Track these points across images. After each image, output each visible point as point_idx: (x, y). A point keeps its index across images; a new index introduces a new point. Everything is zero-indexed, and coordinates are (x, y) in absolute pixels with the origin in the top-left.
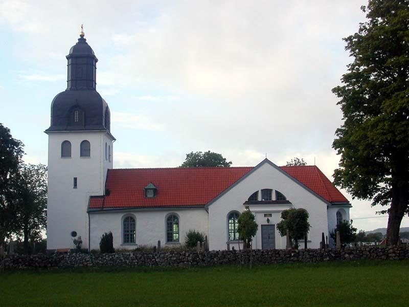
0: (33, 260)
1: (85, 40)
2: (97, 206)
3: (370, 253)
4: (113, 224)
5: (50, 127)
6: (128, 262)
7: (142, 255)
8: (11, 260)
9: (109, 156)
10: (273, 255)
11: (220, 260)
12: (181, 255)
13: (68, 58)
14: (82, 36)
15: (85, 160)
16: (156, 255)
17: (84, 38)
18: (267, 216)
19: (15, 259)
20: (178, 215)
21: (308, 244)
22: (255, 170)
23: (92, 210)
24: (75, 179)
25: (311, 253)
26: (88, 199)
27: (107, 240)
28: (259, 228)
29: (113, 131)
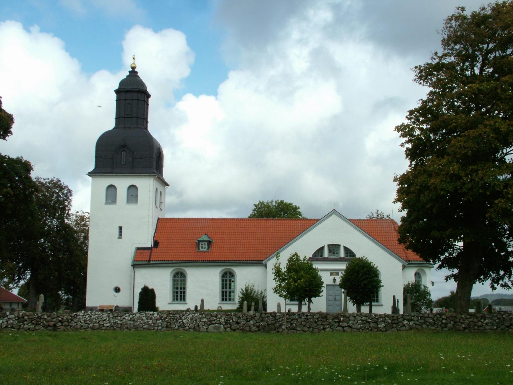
0: (41, 318)
1: (137, 72)
2: (144, 259)
3: (433, 320)
4: (160, 281)
5: (94, 170)
6: (151, 322)
7: (168, 315)
8: (15, 317)
9: (160, 203)
10: (320, 319)
11: (257, 323)
12: (212, 316)
13: (117, 92)
14: (133, 68)
15: (132, 207)
16: (183, 315)
17: (136, 70)
18: (334, 275)
19: (21, 317)
20: (234, 271)
21: (373, 308)
22: (321, 222)
23: (137, 263)
24: (121, 228)
25: (363, 318)
26: (133, 250)
27: (147, 297)
28: (324, 289)
29: (167, 175)
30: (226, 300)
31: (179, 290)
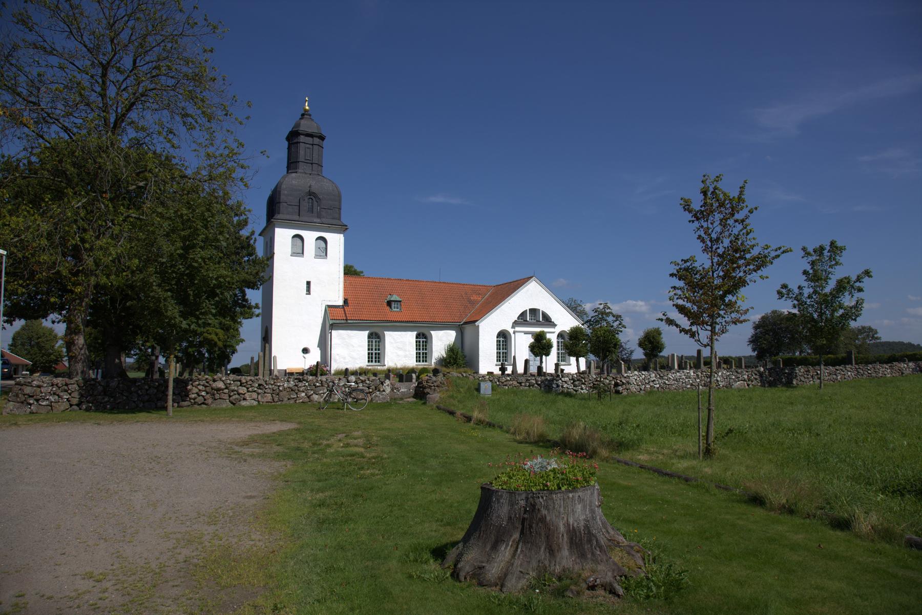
24: (308, 283)
31: (374, 352)
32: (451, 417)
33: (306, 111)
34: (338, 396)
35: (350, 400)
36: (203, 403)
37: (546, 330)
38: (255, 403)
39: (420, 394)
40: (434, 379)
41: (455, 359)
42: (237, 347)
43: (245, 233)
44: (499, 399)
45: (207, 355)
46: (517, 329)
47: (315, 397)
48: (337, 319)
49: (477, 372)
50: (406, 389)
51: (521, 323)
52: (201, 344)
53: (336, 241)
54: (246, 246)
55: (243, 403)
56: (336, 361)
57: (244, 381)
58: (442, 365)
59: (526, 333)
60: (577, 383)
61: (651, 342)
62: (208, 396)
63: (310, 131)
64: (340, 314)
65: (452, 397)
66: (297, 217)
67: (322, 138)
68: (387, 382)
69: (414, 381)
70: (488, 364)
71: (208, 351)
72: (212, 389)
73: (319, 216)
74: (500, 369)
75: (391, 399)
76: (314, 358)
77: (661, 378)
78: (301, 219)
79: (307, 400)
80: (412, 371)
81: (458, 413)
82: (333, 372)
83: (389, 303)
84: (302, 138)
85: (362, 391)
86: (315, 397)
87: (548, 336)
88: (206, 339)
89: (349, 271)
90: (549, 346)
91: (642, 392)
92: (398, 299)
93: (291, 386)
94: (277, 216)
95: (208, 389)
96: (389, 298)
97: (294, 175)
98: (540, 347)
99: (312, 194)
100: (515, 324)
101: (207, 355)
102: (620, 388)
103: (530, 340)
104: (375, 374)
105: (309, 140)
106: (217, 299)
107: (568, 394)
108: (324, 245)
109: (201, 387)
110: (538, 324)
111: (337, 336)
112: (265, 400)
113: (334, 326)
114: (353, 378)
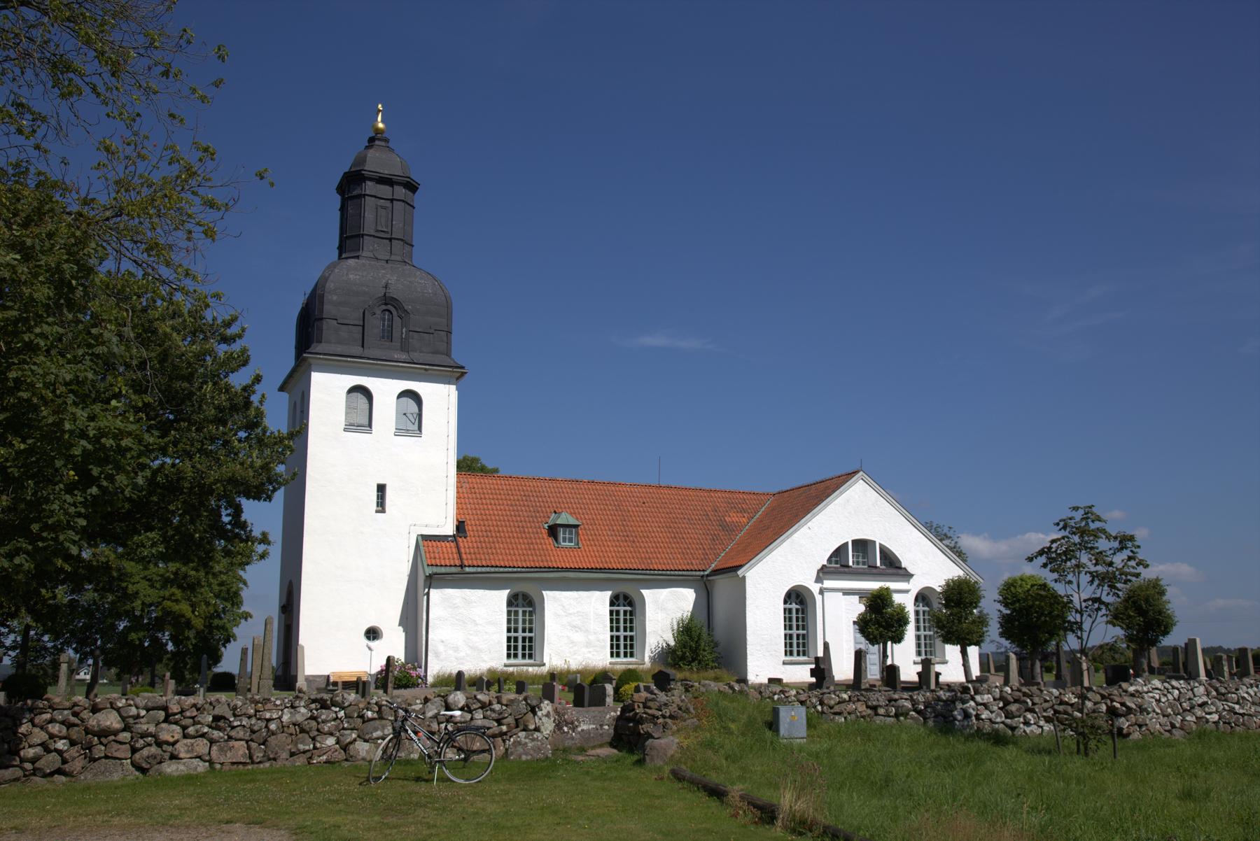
24: (381, 489)
30: (516, 656)
31: (520, 634)
32: (714, 804)
33: (378, 131)
34: (418, 746)
35: (451, 754)
36: (59, 772)
37: (893, 585)
38: (202, 767)
39: (629, 736)
40: (662, 697)
41: (695, 651)
42: (235, 630)
43: (238, 380)
44: (829, 751)
45: (170, 647)
46: (828, 584)
47: (362, 748)
48: (439, 566)
49: (743, 680)
50: (593, 723)
51: (835, 574)
52: (159, 624)
53: (440, 400)
54: (241, 406)
55: (170, 768)
56: (437, 655)
57: (175, 708)
58: (668, 665)
59: (847, 592)
60: (1013, 708)
61: (1141, 612)
62: (74, 751)
63: (386, 171)
64: (448, 554)
65: (709, 745)
66: (357, 350)
67: (412, 187)
68: (547, 706)
69: (609, 700)
70: (766, 659)
71: (174, 639)
72: (87, 731)
73: (405, 347)
74: (813, 673)
75: (555, 750)
76: (394, 645)
77: (1221, 696)
78: (367, 353)
79: (341, 755)
80: (602, 676)
81: (736, 790)
82: (430, 680)
83: (553, 531)
84: (370, 188)
85: (480, 731)
86: (362, 748)
87: (897, 599)
88: (167, 612)
89: (466, 466)
90: (902, 620)
91: (1178, 734)
92: (572, 521)
93: (299, 718)
94: (316, 347)
95: (75, 733)
96: (552, 519)
97: (352, 262)
98: (880, 622)
99: (390, 303)
100: (823, 573)
101: (170, 647)
102: (1124, 723)
103: (857, 608)
104: (521, 686)
105: (385, 190)
106: (94, 490)
107: (997, 739)
108: (415, 408)
109: (55, 728)
110: (871, 572)
111: (441, 600)
112: (229, 757)
113: (435, 580)
114: (459, 698)
